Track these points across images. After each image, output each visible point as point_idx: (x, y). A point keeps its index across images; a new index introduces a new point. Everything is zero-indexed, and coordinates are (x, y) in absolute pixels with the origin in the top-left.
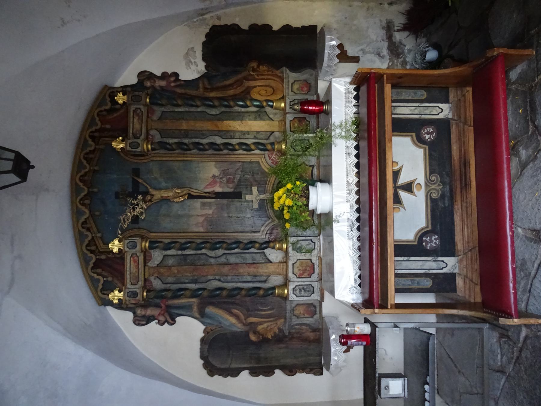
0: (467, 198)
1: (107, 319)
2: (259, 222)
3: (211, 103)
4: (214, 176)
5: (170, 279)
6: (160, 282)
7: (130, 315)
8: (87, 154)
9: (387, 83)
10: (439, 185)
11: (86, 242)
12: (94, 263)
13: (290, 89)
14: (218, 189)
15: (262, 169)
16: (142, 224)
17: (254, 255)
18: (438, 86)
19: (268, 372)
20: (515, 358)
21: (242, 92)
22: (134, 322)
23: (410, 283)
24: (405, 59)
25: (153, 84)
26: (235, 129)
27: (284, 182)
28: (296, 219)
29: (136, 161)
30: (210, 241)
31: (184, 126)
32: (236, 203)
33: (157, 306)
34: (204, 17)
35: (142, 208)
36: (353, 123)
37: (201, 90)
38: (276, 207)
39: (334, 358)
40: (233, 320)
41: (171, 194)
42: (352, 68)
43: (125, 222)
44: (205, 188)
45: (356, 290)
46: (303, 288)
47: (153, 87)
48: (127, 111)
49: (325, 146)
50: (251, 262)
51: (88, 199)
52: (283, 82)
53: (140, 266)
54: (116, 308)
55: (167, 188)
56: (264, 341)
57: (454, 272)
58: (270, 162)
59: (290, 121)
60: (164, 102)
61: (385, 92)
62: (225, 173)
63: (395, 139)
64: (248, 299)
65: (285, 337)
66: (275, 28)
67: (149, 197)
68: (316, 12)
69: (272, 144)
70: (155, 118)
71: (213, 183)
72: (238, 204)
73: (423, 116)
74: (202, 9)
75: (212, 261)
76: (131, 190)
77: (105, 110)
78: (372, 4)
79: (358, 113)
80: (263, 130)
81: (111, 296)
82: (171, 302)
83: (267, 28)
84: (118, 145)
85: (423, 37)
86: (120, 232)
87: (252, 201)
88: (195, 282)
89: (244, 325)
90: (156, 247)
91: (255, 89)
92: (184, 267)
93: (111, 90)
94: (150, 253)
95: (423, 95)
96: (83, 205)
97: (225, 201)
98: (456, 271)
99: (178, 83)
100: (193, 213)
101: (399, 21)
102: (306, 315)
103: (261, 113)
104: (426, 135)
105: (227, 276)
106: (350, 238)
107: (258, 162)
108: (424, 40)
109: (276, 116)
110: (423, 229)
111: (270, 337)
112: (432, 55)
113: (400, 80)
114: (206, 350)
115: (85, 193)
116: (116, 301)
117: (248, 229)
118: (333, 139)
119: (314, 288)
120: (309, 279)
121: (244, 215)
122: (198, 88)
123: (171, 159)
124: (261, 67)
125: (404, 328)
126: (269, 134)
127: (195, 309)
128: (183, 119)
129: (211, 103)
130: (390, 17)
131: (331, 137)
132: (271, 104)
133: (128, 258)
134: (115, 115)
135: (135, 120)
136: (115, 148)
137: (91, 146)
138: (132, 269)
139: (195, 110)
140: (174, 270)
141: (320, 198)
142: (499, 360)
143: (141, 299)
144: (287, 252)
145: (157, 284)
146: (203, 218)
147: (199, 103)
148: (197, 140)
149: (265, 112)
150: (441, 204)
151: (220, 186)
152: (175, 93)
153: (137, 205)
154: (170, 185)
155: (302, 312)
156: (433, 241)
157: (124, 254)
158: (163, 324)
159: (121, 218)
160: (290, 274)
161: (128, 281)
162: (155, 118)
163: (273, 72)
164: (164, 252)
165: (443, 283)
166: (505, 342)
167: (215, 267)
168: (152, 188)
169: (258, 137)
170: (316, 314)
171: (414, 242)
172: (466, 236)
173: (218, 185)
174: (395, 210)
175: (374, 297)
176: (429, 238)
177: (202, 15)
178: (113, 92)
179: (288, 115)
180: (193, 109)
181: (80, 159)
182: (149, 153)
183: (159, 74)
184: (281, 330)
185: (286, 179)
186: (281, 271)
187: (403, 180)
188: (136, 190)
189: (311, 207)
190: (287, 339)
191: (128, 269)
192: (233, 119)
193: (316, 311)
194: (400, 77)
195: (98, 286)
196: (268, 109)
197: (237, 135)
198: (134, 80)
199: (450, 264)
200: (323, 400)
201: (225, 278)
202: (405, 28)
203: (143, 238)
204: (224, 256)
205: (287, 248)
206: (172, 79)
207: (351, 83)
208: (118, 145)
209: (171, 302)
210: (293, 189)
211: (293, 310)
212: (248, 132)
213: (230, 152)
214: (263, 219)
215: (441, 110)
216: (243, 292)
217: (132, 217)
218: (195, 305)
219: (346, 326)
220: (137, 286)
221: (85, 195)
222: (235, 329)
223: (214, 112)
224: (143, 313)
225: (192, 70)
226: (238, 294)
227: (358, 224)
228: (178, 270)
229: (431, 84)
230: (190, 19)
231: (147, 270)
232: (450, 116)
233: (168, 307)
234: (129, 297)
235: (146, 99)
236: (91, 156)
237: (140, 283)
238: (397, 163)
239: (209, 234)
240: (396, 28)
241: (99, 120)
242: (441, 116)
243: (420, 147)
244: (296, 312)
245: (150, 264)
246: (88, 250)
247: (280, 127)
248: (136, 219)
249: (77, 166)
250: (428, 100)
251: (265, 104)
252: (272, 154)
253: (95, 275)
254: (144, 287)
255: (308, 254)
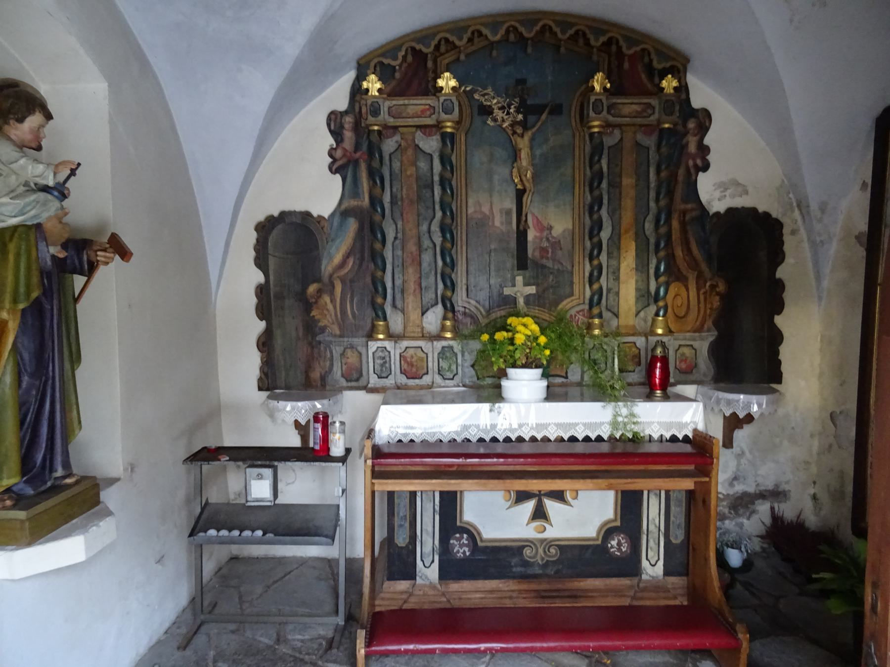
0: (524, 598)
1: (338, 72)
2: (483, 295)
3: (662, 222)
4: (550, 228)
5: (396, 165)
6: (392, 150)
7: (342, 104)
8: (584, 34)
9: (695, 483)
10: (543, 559)
11: (452, 38)
12: (420, 51)
13: (683, 343)
14: (531, 235)
15: (562, 301)
16: (478, 120)
17: (433, 289)
18: (691, 563)
19: (263, 311)
20: (301, 657)
21: (679, 270)
22: (333, 113)
23: (401, 514)
24: (728, 518)
25: (691, 132)
26: (622, 258)
27: (548, 332)
28: (494, 350)
29: (573, 109)
30: (455, 223)
31: (628, 181)
32: (511, 262)
33: (357, 148)
34: (796, 209)
35: (503, 121)
36: (635, 434)
37: (683, 207)
38: (511, 320)
39: (289, 406)
40: (338, 259)
41: (524, 163)
42: (717, 432)
43: (483, 95)
44: (533, 215)
45: (393, 436)
46: (385, 362)
47: (686, 133)
48: (649, 94)
49: (600, 392)
50: (423, 285)
51: (515, 37)
52: (695, 332)
53: (416, 119)
54: (353, 85)
55: (532, 156)
56: (307, 305)
57: (418, 578)
58: (573, 312)
59: (635, 343)
60: (664, 150)
61: (684, 479)
62: (556, 244)
63: (611, 495)
64: (369, 280)
65: (314, 335)
66: (778, 320)
67: (519, 130)
68: (803, 383)
69: (600, 316)
70: (640, 137)
71: (540, 227)
72: (509, 265)
73: (644, 537)
74: (808, 206)
75: (424, 228)
76: (529, 102)
77: (651, 61)
78: (814, 469)
79: (650, 441)
80: (621, 301)
81: (373, 77)
82: (363, 166)
83: (779, 307)
84: (598, 82)
85: (762, 547)
86: (468, 89)
87: (514, 285)
88: (393, 202)
89: (331, 276)
90: (444, 143)
91: (683, 289)
92: (415, 186)
93: (681, 68)
94: (435, 134)
95: (676, 538)
96: (508, 31)
97: (513, 244)
98: (419, 581)
99: (692, 171)
100: (496, 199)
101: (788, 511)
102: (344, 367)
103: (646, 298)
104: (616, 541)
105: (403, 249)
106: (466, 428)
107: (572, 294)
108: (758, 548)
109: (642, 323)
110: (479, 534)
111: (313, 313)
112: (735, 558)
113: (700, 503)
114: (294, 220)
115: (526, 35)
116: (365, 85)
117: (472, 280)
118: (613, 404)
119: (387, 377)
120: (398, 371)
121: (493, 273)
122: (685, 201)
123: (577, 163)
124: (717, 298)
125: (338, 506)
126: (615, 310)
127: (354, 203)
128: (638, 180)
129: (662, 222)
130: (794, 495)
131: (616, 399)
132: (661, 313)
133: (429, 102)
134: (643, 76)
135: (635, 107)
136: (593, 77)
137: (597, 40)
138: (412, 107)
139: (651, 196)
140: (411, 171)
141: (524, 384)
142: (296, 637)
143: (368, 122)
144: (439, 337)
145: (389, 145)
146: (488, 213)
147: (662, 203)
148: (605, 201)
149: (648, 305)
150: (514, 561)
151: (536, 237)
152: (678, 166)
153: (508, 113)
154: (537, 161)
155: (350, 361)
156: (461, 549)
157: (435, 95)
158: (330, 155)
159: (489, 90)
160: (405, 343)
161: (394, 102)
162: (640, 137)
163: (710, 316)
164: (437, 154)
165: (398, 561)
166: (321, 644)
167: (414, 231)
168: (534, 134)
169: (611, 296)
170: (347, 381)
171: (461, 522)
172: (469, 596)
173: (538, 234)
174: (508, 494)
175: (390, 460)
176: (466, 542)
177: (799, 206)
178: (679, 72)
179: (643, 339)
180: (652, 194)
181: (576, 24)
182: (586, 129)
183: (707, 140)
184: (323, 330)
185: (553, 335)
186: (409, 329)
187: (551, 505)
188: (530, 111)
189: (511, 372)
190: (310, 338)
191: (412, 102)
192: (637, 255)
193: (351, 381)
194: (706, 502)
195: (386, 58)
196: (653, 309)
197: (614, 262)
198: (697, 102)
199: (428, 572)
200: (222, 390)
201: (400, 247)
202: (776, 519)
203: (458, 123)
204: (431, 245)
205: (446, 339)
206: (699, 162)
207: (695, 430)
208: (598, 82)
209: (363, 166)
210: (538, 345)
211: (352, 347)
212: (617, 279)
213: (587, 252)
214: (487, 303)
215: (653, 563)
216: (379, 273)
217: (490, 106)
218: (360, 203)
219: (341, 422)
220: (387, 116)
221: (521, 34)
222: (324, 263)
223: (649, 226)
224: (346, 126)
225: (713, 192)
226: (375, 264)
227: (488, 439)
228: (411, 176)
229: (694, 549)
230: (792, 187)
231: (410, 129)
232: (644, 577)
233: (356, 163)
234: (372, 105)
235: (667, 123)
236: (581, 41)
237: (392, 120)
238: (576, 498)
239: (464, 223)
240: (776, 506)
241: (636, 52)
242: (645, 563)
243: (599, 533)
244: (349, 353)
245: (419, 134)
246: (440, 41)
247: (626, 326)
248: (486, 111)
249: (565, 20)
250: (668, 543)
251: (661, 304)
252: (584, 315)
253: (403, 53)
254: (386, 127)
255: (436, 369)
